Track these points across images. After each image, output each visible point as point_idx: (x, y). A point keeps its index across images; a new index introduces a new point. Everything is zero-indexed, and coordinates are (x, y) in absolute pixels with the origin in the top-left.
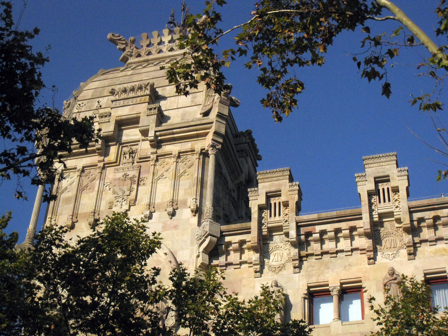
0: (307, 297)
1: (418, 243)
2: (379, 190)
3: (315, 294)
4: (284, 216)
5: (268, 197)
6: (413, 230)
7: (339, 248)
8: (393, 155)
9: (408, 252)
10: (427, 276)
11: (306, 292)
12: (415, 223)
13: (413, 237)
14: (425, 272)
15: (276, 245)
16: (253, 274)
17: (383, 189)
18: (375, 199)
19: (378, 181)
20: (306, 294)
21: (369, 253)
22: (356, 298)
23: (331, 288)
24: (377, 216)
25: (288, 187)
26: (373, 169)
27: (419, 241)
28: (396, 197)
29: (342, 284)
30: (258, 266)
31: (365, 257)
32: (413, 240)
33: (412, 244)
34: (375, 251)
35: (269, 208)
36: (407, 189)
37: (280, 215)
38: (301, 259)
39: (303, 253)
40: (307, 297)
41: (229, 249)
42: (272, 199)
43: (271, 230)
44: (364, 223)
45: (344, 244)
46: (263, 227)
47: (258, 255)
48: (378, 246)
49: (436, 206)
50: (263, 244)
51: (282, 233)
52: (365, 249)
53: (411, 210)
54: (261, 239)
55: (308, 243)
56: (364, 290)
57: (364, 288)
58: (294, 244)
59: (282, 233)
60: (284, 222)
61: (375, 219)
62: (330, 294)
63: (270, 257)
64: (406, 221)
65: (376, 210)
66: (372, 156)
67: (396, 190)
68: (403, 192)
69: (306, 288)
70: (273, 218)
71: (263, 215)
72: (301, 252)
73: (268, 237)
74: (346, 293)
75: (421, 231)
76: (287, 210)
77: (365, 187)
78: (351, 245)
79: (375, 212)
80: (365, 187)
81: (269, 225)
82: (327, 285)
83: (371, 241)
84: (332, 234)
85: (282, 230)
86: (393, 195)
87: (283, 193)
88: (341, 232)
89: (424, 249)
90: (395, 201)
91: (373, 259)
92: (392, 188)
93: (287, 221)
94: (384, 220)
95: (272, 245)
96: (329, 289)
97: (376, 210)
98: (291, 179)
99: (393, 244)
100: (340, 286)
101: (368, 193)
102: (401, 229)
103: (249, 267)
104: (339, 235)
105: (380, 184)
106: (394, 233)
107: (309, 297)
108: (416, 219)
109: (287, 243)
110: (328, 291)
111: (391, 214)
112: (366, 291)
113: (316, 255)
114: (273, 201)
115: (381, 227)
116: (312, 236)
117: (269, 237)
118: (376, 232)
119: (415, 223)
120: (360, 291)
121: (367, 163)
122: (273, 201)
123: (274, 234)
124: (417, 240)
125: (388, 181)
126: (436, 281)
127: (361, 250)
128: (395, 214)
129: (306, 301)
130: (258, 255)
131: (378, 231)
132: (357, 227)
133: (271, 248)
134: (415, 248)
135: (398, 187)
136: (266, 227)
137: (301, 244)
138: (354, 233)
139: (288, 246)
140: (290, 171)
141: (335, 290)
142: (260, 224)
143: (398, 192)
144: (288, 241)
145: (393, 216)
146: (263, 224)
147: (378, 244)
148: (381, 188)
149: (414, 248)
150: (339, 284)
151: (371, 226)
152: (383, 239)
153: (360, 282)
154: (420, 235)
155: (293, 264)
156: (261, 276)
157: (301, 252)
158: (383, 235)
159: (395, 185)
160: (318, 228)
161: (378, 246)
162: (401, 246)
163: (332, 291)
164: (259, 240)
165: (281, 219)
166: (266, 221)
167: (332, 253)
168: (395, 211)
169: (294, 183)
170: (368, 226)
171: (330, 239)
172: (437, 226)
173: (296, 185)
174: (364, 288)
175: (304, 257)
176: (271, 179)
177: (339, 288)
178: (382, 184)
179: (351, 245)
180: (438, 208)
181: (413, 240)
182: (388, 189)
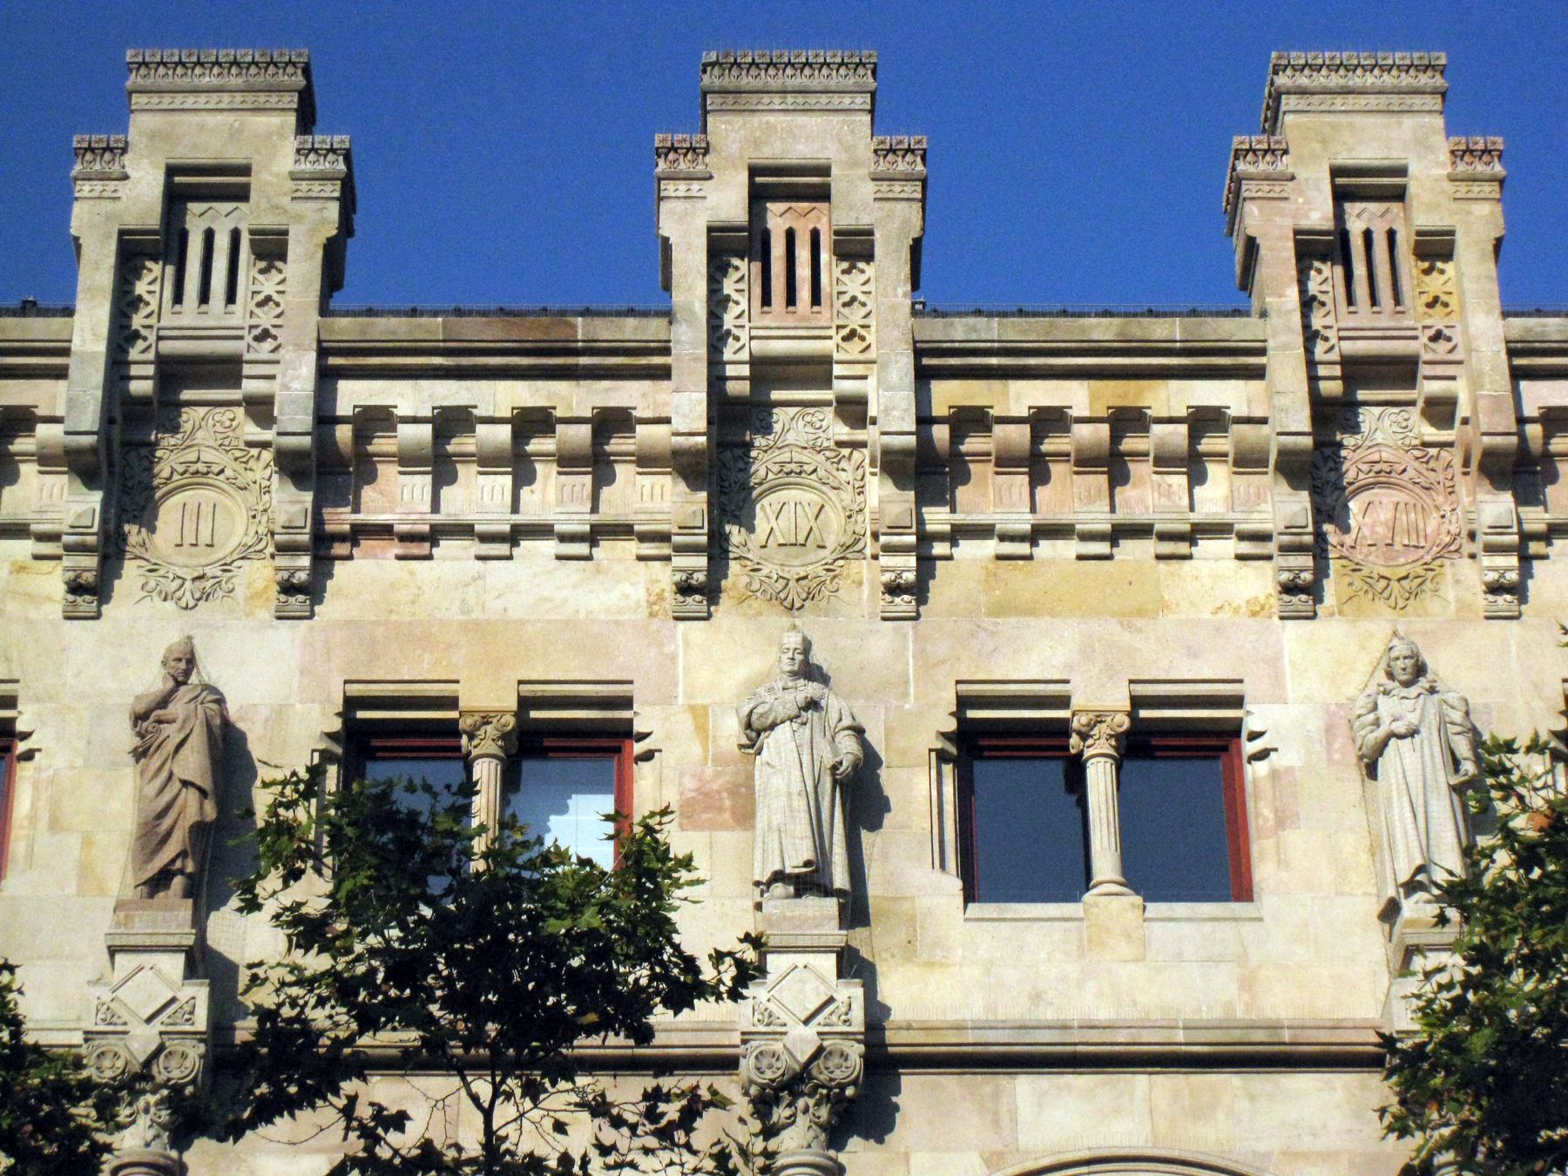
0: (339, 750)
1: (940, 537)
2: (183, 236)
3: (984, 742)
4: (252, 306)
5: (176, 197)
6: (927, 470)
7: (1122, 516)
8: (861, 64)
9: (71, 575)
10: (1144, 714)
11: (336, 725)
12: (344, 433)
13: (921, 502)
14: (356, 690)
15: (192, 457)
16: (1482, 601)
17: (209, 236)
18: (741, 278)
19: (1348, 187)
20: (331, 736)
21: (680, 561)
22: (592, 786)
23: (1084, 720)
24: (745, 370)
25: (292, 156)
26: (175, 125)
27: (1542, 527)
28: (268, 285)
29: (526, 703)
30: (91, 561)
31: (1260, 581)
32: (318, 521)
33: (304, 538)
34: (716, 551)
35: (175, 258)
36: (916, 248)
37: (231, 297)
38: (324, 548)
39: (340, 519)
40: (339, 750)
41: (370, 448)
42: (194, 208)
43: (177, 373)
44: (71, 403)
45: (555, 496)
46: (134, 354)
47: (95, 499)
48: (131, 529)
49: (994, 361)
50: (124, 444)
51: (235, 395)
52: (664, 537)
53: (334, 361)
54: (118, 415)
55: (363, 468)
56: (21, 747)
57: (642, 737)
58: (293, 466)
59: (235, 395)
60: (837, 339)
61: (733, 388)
62: (459, 748)
63: (156, 517)
64: (295, 417)
65: (744, 335)
66: (225, 55)
67: (855, 247)
68: (303, 267)
69: (339, 705)
70: (189, 312)
71: (141, 288)
72: (328, 513)
73: (155, 405)
74: (541, 753)
75: (371, 477)
76: (275, 277)
77: (693, 211)
78: (515, 509)
79: (140, 344)
80: (693, 211)
81: (167, 347)
82: (1063, 702)
83: (703, 495)
84: (1020, 436)
85: (235, 380)
86: (837, 272)
87: (258, 182)
88: (1145, 429)
89: (360, 577)
90: (260, 305)
91: (91, 592)
92: (252, 232)
93: (852, 335)
94: (776, 395)
95: (169, 459)
96: (456, 721)
97: (744, 338)
98: (306, 120)
99: (190, 527)
100: (516, 714)
101: (1297, 242)
102: (267, 455)
103: (1159, 557)
104: (616, 444)
105: (774, 208)
106: (229, 472)
107: (346, 751)
108: (1535, 413)
109: (254, 451)
110: (450, 729)
111: (816, 370)
112: (648, 756)
113: (1086, 537)
114: (197, 218)
115: (757, 432)
116: (1146, 429)
117: (161, 411)
118: (133, 454)
119: (344, 433)
120: (617, 750)
121: (717, 82)
122: (197, 218)
123: (187, 395)
124: (938, 518)
125: (241, 194)
126: (1011, 742)
127: (644, 537)
128: (837, 370)
129: (948, 769)
130: (95, 499)
131: (144, 451)
132: (39, 412)
133: (762, 473)
134: (927, 565)
135: (1452, 233)
136: (151, 355)
137: (328, 466)
138: (536, 445)
139: (263, 467)
140: (307, 72)
141: (1103, 729)
142: (121, 336)
143: (283, 257)
144: (265, 445)
145: (826, 381)
146: (136, 335)
147: (134, 519)
148: (1355, 227)
149: (316, 559)
150: (512, 704)
151: (710, 422)
152: (762, 495)
153: (1237, 702)
154: (357, 497)
155: (67, 569)
156: (917, 618)
157: (328, 513)
158: (165, 474)
159: (269, 221)
160: (1023, 397)
161: (131, 529)
162: (250, 540)
163: (471, 737)
164: (108, 419)
165: (234, 321)
166: (152, 321)
167: (486, 538)
168: (1425, 356)
169: (320, 139)
170: (89, 417)
171: (488, 461)
172: (610, 464)
173: (332, 150)
174: (642, 737)
175: (341, 538)
176: (800, 99)
177: (510, 721)
178: (203, 206)
179: (515, 509)
180: (1000, 367)
181: (921, 521)
182: (815, 235)
